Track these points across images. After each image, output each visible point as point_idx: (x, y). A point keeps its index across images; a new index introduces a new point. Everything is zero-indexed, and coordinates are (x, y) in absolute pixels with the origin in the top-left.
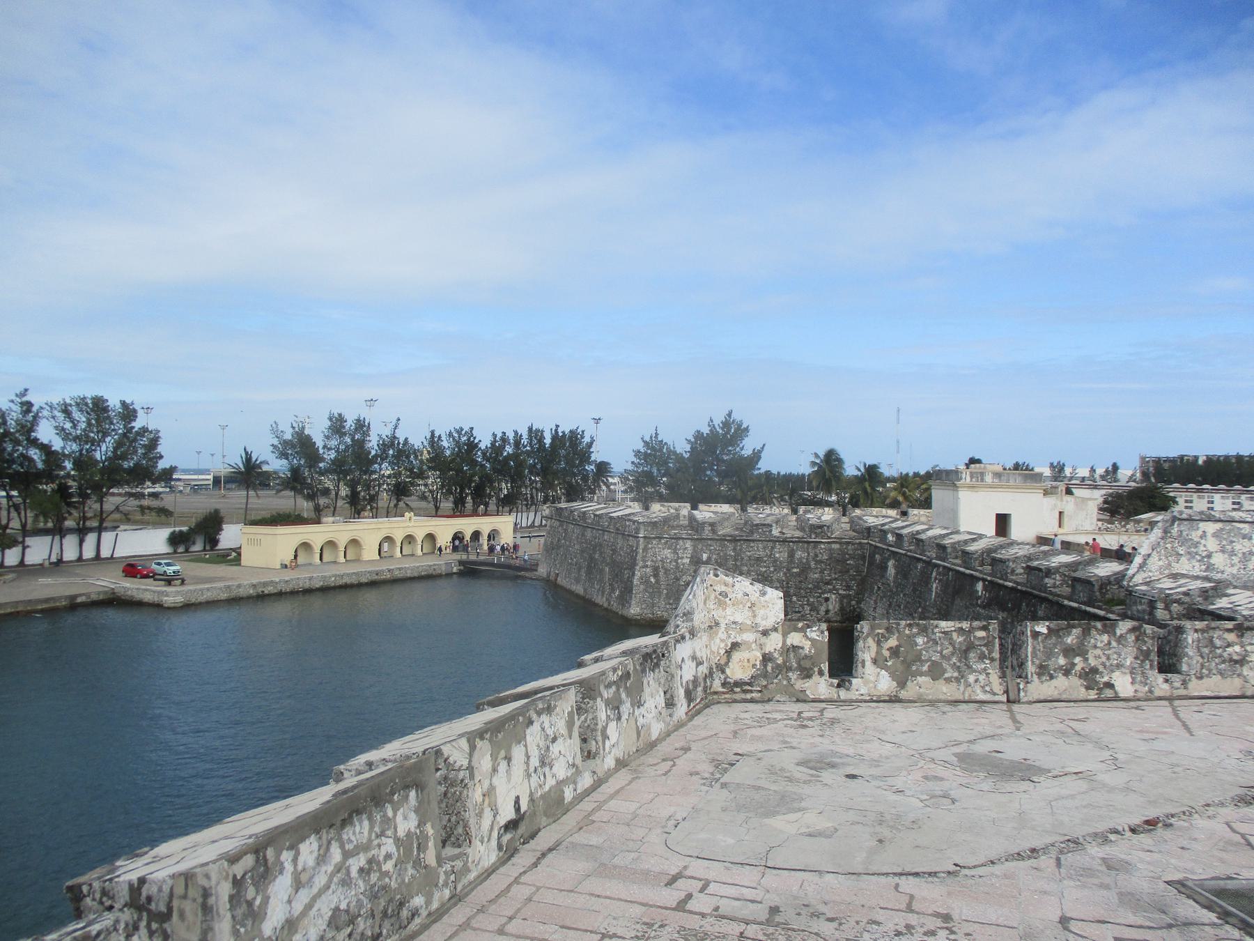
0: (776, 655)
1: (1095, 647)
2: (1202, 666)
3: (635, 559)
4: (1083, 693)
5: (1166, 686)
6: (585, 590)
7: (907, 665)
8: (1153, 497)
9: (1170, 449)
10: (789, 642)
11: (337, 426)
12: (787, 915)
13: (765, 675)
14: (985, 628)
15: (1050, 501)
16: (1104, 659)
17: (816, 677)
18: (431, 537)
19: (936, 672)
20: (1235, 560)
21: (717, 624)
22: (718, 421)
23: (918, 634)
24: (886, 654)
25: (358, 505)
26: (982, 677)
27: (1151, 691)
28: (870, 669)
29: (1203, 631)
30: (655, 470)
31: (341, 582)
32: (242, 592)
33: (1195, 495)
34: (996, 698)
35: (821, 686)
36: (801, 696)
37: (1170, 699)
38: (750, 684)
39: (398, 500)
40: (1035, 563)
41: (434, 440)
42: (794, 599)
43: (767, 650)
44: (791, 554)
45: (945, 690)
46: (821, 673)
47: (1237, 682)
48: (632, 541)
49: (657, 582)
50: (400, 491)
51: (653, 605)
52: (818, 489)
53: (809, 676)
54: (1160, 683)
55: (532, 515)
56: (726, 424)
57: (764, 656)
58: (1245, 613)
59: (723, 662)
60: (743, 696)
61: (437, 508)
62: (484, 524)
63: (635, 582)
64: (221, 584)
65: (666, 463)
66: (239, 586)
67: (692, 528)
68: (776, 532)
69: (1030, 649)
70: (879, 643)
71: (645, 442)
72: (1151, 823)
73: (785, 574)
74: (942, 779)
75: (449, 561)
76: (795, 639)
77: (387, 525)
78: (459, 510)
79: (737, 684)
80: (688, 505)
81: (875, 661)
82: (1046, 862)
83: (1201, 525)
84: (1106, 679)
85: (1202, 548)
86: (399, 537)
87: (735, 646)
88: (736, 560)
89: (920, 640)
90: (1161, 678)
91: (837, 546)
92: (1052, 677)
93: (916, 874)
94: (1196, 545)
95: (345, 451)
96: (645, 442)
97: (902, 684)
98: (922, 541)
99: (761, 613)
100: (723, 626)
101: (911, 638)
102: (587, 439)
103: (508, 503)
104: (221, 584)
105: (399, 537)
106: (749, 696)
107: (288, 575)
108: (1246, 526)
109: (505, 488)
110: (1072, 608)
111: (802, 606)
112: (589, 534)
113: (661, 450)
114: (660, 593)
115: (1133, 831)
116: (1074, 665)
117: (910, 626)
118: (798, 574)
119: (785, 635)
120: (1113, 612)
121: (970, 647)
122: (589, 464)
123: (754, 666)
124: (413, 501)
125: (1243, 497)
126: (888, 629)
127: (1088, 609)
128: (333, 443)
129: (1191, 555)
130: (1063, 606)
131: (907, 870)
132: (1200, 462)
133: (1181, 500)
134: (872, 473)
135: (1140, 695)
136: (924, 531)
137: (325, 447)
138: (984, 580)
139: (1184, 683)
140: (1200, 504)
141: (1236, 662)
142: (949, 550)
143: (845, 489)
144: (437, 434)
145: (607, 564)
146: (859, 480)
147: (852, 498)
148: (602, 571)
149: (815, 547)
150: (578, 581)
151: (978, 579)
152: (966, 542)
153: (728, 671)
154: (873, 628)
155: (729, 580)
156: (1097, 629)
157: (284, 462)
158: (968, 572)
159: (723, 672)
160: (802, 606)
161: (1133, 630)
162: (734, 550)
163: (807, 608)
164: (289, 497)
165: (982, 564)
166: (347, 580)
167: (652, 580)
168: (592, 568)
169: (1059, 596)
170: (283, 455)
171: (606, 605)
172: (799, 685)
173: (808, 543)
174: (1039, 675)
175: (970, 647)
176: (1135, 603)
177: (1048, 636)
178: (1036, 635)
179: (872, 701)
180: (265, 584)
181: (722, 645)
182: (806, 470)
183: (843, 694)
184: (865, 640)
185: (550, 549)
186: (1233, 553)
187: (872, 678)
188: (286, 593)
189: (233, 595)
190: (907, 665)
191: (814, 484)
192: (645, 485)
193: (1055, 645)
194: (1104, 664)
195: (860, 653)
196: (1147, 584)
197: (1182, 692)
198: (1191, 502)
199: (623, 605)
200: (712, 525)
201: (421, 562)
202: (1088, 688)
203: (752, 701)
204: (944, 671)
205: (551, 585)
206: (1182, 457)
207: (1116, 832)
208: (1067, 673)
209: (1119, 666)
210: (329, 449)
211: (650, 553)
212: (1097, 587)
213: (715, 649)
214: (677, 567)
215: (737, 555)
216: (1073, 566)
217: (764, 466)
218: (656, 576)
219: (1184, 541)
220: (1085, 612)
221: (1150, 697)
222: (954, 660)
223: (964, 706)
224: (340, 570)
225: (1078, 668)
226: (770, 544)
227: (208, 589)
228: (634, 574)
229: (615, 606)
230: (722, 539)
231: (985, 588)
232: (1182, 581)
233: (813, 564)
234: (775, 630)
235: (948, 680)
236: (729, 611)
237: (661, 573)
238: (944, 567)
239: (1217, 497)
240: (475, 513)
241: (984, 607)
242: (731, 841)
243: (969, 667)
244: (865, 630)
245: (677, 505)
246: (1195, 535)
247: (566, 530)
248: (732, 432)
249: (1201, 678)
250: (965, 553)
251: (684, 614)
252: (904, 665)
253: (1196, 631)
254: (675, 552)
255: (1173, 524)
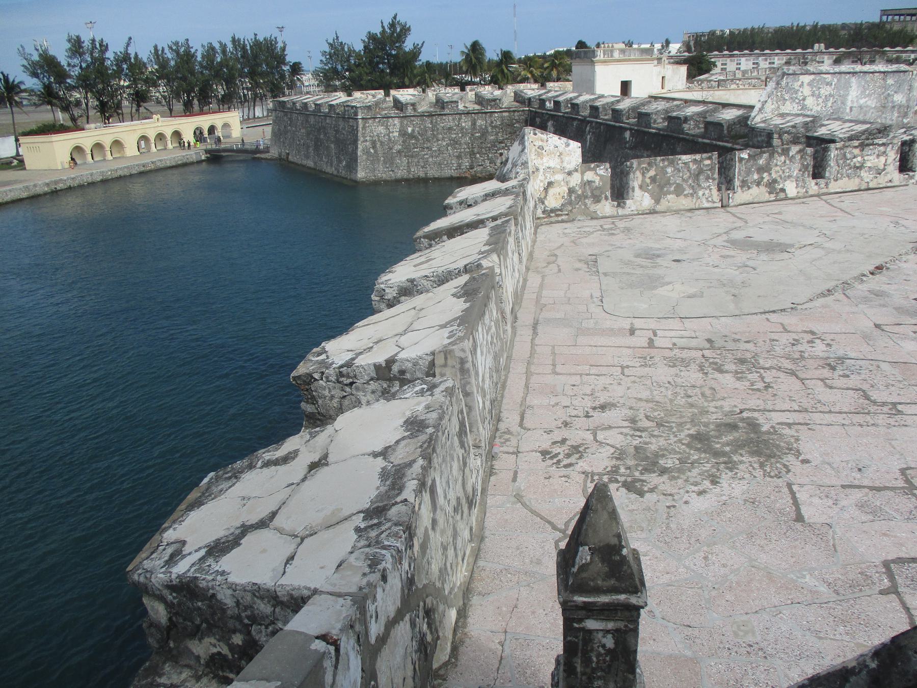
0: (577, 188)
1: (776, 165)
2: (838, 172)
3: (357, 136)
4: (767, 197)
5: (816, 188)
6: (315, 163)
7: (661, 187)
8: (701, 63)
9: (704, 27)
10: (585, 179)
11: (76, 47)
12: (719, 343)
13: (570, 203)
14: (710, 158)
15: (659, 68)
16: (781, 173)
17: (603, 201)
18: (177, 134)
19: (679, 191)
20: (820, 100)
21: (537, 170)
22: (387, 21)
23: (668, 165)
24: (648, 181)
25: (108, 110)
26: (707, 192)
27: (807, 192)
28: (638, 192)
29: (841, 149)
30: (339, 67)
31: (116, 175)
32: (38, 190)
33: (728, 60)
34: (715, 205)
35: (607, 207)
36: (595, 216)
37: (818, 196)
38: (560, 210)
39: (139, 106)
40: (674, 114)
41: (157, 54)
42: (478, 156)
43: (571, 185)
44: (474, 124)
45: (685, 202)
46: (606, 198)
47: (857, 181)
48: (351, 122)
49: (376, 152)
50: (140, 98)
51: (375, 170)
52: (466, 73)
53: (599, 201)
54: (812, 186)
55: (246, 110)
56: (392, 25)
57: (569, 189)
58: (841, 136)
59: (542, 196)
60: (556, 219)
61: (171, 110)
62: (217, 119)
63: (359, 153)
64: (21, 186)
65: (348, 60)
66: (35, 186)
67: (398, 109)
68: (461, 107)
69: (737, 170)
70: (643, 174)
71: (329, 44)
72: (879, 268)
73: (470, 138)
74: (733, 257)
75: (198, 152)
76: (589, 176)
77: (141, 127)
78: (188, 110)
79: (552, 211)
80: (382, 92)
81: (641, 187)
82: (839, 295)
83: (801, 77)
84: (781, 186)
85: (800, 94)
86: (152, 136)
87: (550, 184)
88: (433, 131)
89: (669, 170)
90: (813, 182)
91: (506, 114)
92: (749, 188)
93: (774, 312)
94: (796, 92)
95: (88, 66)
96: (329, 44)
97: (657, 201)
98: (577, 105)
99: (567, 159)
100: (542, 171)
101: (664, 168)
102: (280, 45)
103: (227, 102)
104: (21, 186)
105: (152, 136)
106: (560, 219)
107: (73, 174)
108: (829, 76)
109: (221, 91)
110: (704, 143)
111: (483, 161)
112: (312, 120)
113: (343, 49)
114: (379, 160)
115: (872, 274)
116: (763, 178)
117: (663, 160)
118: (480, 138)
119: (583, 174)
120: (738, 144)
121: (700, 172)
122: (285, 64)
123: (563, 197)
124: (151, 105)
125: (760, 58)
126: (649, 164)
127: (721, 143)
128: (76, 61)
129: (792, 100)
130: (697, 143)
131: (767, 310)
132: (808, 28)
133: (719, 64)
134: (507, 56)
135: (800, 195)
136: (576, 98)
137: (69, 65)
138: (631, 130)
139: (827, 185)
140: (731, 66)
141: (858, 168)
142: (601, 110)
143: (486, 72)
144: (160, 48)
145: (332, 142)
146: (499, 64)
147: (492, 77)
148: (328, 148)
149: (491, 116)
150: (307, 157)
151: (626, 129)
152: (613, 103)
153: (546, 202)
154: (639, 164)
155: (544, 137)
156: (778, 153)
157: (35, 80)
158: (617, 124)
159: (543, 203)
160: (483, 161)
161: (800, 151)
162: (431, 123)
163: (487, 162)
164: (47, 111)
165: (628, 118)
166: (120, 173)
167: (372, 151)
168: (318, 145)
169: (693, 136)
170: (35, 75)
171: (335, 173)
172: (593, 207)
173: (486, 113)
174: (742, 187)
175: (700, 172)
176: (756, 136)
177: (748, 160)
178: (741, 159)
179: (639, 214)
180: (56, 182)
181: (542, 184)
182: (458, 58)
183: (621, 211)
184: (634, 173)
185: (278, 135)
186: (819, 96)
187: (639, 199)
188: (74, 187)
189: (32, 193)
190: (661, 187)
191: (464, 69)
192: (332, 79)
193: (752, 166)
194: (780, 176)
195: (631, 182)
196: (764, 122)
197: (825, 190)
198: (726, 64)
199: (351, 172)
200: (413, 105)
201: (172, 154)
202: (770, 193)
203: (563, 221)
204: (684, 190)
205: (283, 164)
206: (712, 33)
207: (864, 275)
208: (758, 184)
209: (789, 177)
210: (74, 66)
211: (368, 130)
212: (725, 128)
213: (537, 187)
214: (390, 140)
215: (434, 126)
216: (702, 114)
217: (423, 58)
218: (374, 147)
219: (789, 89)
220: (716, 145)
221: (807, 196)
222: (690, 181)
223: (697, 212)
224: (110, 166)
225: (765, 180)
226: (457, 117)
227: (10, 191)
228: (357, 148)
229: (343, 173)
230: (422, 115)
231: (632, 135)
232: (789, 118)
233: (490, 129)
234: (576, 170)
235: (686, 196)
236: (545, 160)
237: (378, 145)
238: (597, 123)
239: (743, 60)
240: (202, 113)
241: (631, 149)
242: (646, 306)
243: (699, 186)
244: (635, 166)
245: (373, 92)
246: (796, 85)
247: (290, 119)
248: (396, 33)
249: (837, 180)
250: (614, 111)
251: (522, 164)
252: (659, 188)
253: (837, 149)
254: (387, 128)
255: (782, 78)
